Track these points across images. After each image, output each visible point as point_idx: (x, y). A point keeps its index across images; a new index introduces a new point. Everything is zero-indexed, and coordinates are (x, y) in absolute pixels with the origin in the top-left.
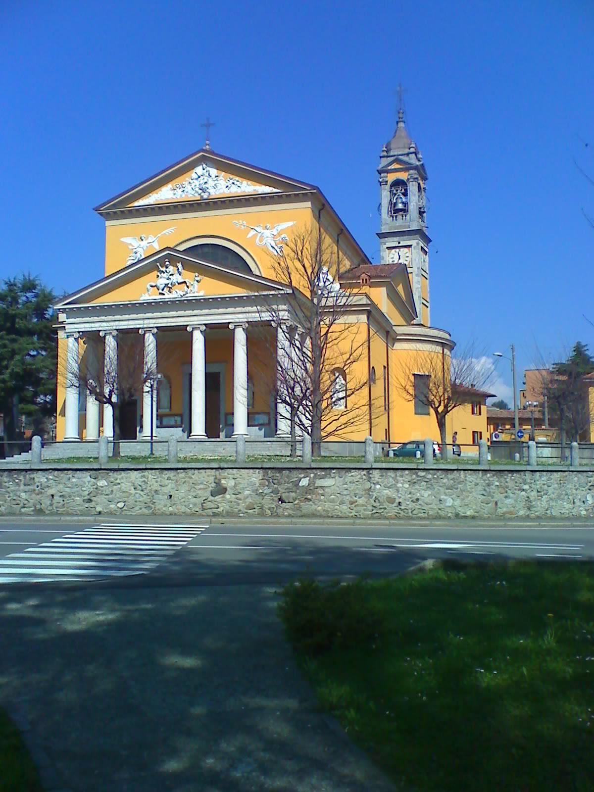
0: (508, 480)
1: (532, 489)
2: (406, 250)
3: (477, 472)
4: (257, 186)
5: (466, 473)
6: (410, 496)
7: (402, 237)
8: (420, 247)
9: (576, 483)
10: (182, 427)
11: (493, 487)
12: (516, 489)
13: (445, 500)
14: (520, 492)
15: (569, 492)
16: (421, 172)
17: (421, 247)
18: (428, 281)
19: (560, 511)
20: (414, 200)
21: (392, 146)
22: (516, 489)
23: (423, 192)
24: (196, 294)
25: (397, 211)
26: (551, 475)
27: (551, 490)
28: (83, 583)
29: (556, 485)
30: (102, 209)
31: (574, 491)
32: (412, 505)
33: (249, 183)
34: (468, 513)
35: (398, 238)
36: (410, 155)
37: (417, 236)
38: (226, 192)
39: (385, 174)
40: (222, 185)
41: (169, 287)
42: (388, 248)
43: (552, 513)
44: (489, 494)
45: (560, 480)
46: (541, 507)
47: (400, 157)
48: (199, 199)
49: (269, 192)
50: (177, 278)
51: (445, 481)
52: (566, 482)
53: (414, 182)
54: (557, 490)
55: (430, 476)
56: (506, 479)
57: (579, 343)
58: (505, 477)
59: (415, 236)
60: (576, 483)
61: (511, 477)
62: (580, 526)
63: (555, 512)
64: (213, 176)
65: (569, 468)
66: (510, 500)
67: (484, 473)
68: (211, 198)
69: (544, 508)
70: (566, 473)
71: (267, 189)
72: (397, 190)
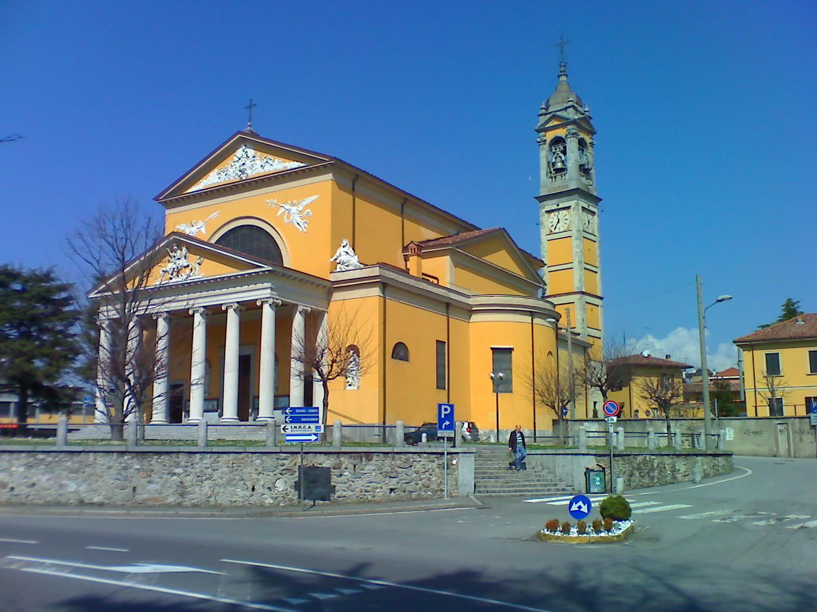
0: (152, 462)
1: (188, 473)
2: (565, 212)
3: (111, 454)
4: (287, 163)
5: (96, 456)
6: (25, 480)
7: (561, 199)
8: (581, 208)
9: (258, 466)
10: (217, 411)
11: (131, 470)
12: (163, 473)
13: (67, 485)
14: (169, 476)
15: (246, 477)
16: (585, 124)
17: (583, 207)
18: (597, 244)
19: (230, 499)
20: (573, 157)
21: (551, 102)
22: (163, 473)
23: (590, 148)
24: (197, 277)
25: (558, 171)
26: (219, 457)
27: (216, 475)
28: (135, 564)
29: (225, 469)
30: (161, 198)
31: (256, 476)
32: (26, 490)
33: (281, 160)
34: (96, 500)
35: (557, 200)
36: (568, 110)
37: (576, 196)
38: (261, 171)
39: (544, 133)
40: (256, 163)
41: (178, 271)
42: (549, 212)
43: (216, 501)
44: (126, 479)
45: (233, 463)
46: (201, 494)
47: (558, 113)
48: (239, 180)
49: (297, 166)
50: (183, 262)
51: (69, 464)
52: (242, 465)
53: (572, 138)
54: (226, 474)
55: (50, 459)
56: (150, 461)
57: (789, 300)
58: (149, 459)
59: (574, 196)
60: (258, 466)
61: (157, 459)
62: (189, 516)
63: (222, 500)
64: (251, 157)
65: (246, 449)
66: (154, 485)
67: (120, 454)
68: (248, 178)
69: (206, 494)
70: (243, 455)
71: (295, 165)
72: (556, 149)
